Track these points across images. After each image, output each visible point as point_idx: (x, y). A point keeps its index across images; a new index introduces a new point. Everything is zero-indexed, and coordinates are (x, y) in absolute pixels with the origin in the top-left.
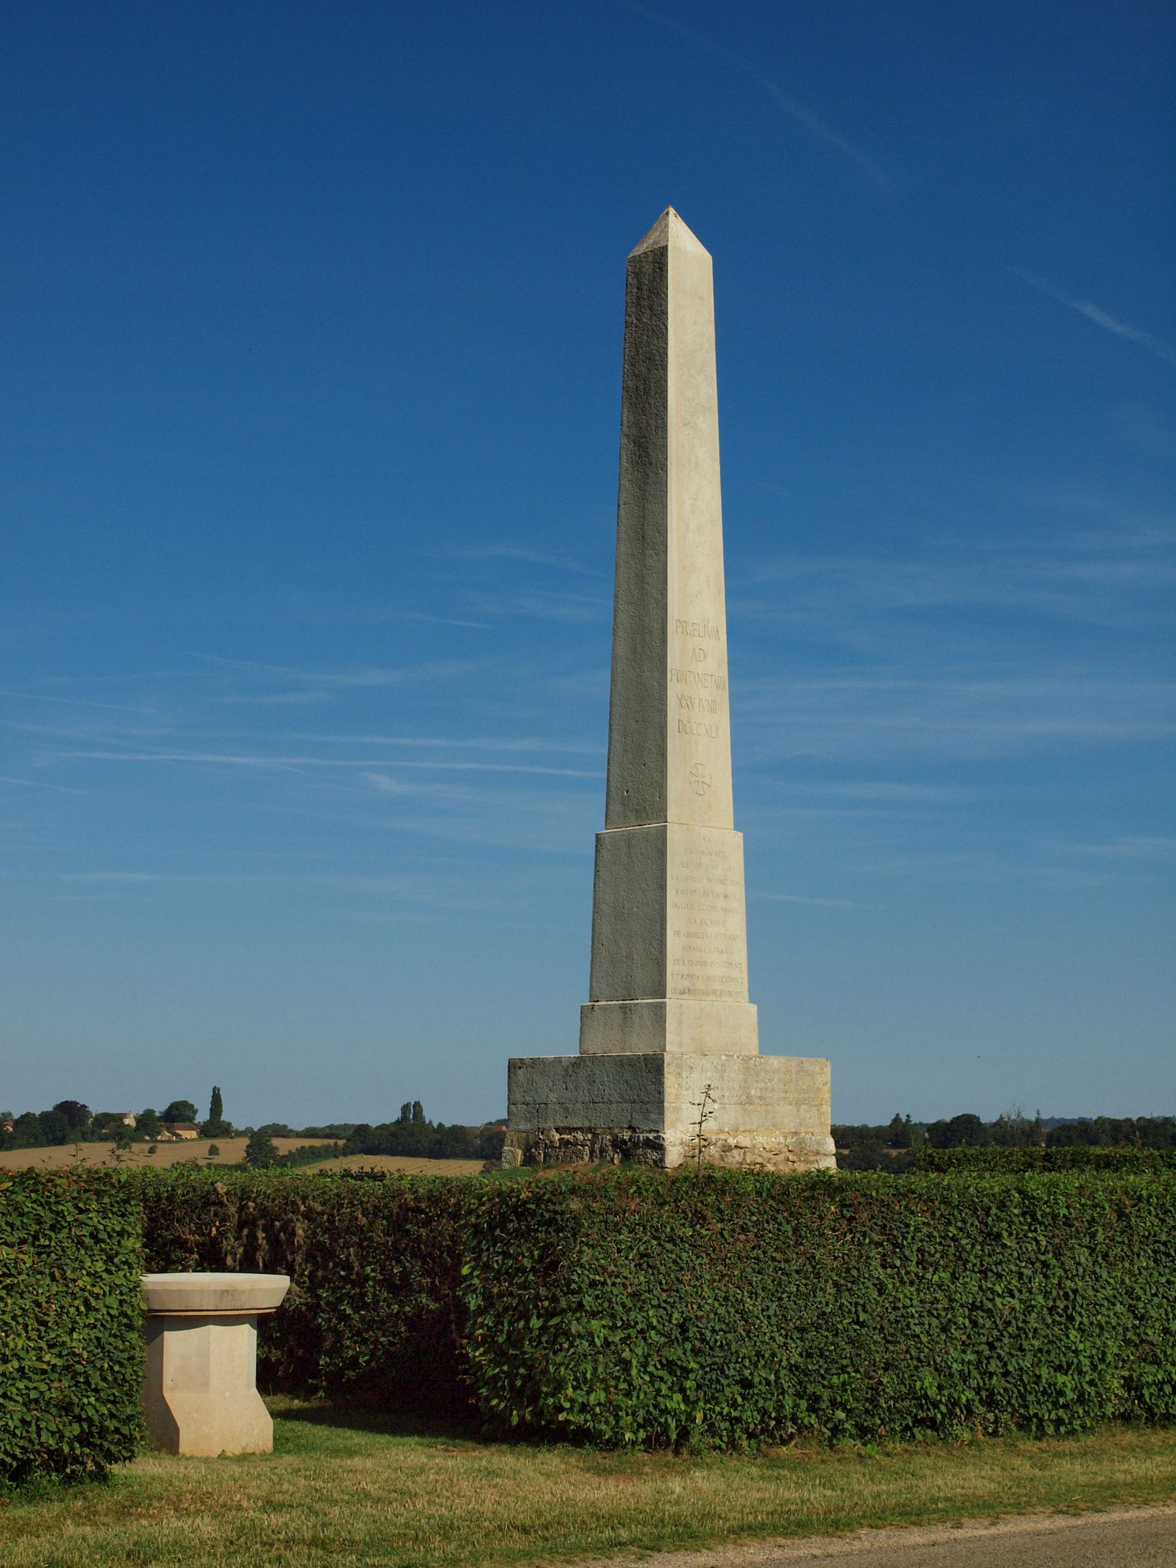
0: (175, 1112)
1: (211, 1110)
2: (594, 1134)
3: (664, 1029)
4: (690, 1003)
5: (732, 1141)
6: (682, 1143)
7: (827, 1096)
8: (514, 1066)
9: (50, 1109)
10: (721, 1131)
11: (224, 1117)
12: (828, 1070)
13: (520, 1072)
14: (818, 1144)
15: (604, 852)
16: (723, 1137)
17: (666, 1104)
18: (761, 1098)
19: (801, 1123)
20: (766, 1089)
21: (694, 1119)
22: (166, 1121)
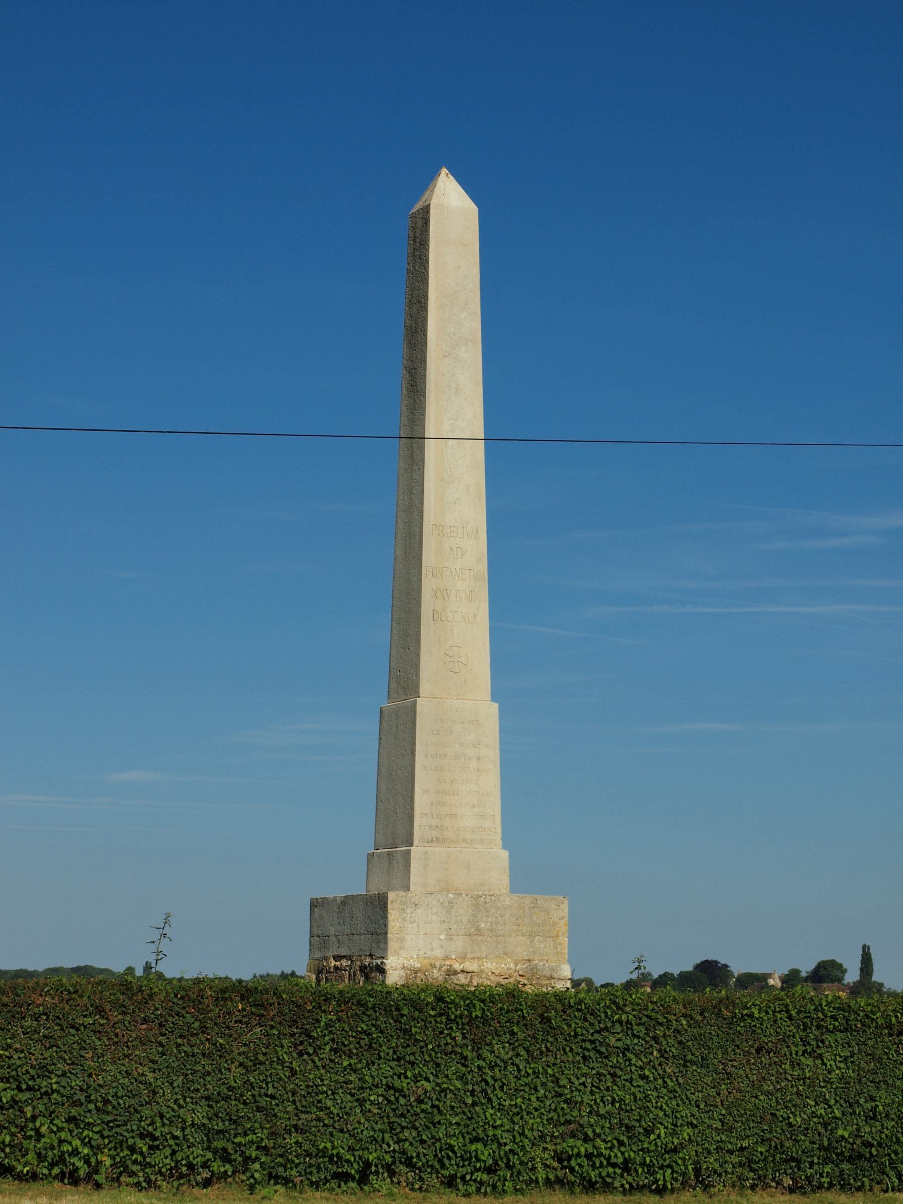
0: (822, 972)
1: (862, 970)
2: (352, 961)
3: (409, 872)
4: (437, 851)
5: (457, 967)
6: (403, 968)
7: (564, 928)
8: (314, 904)
9: (690, 968)
10: (447, 958)
11: (876, 977)
12: (565, 906)
13: (316, 909)
14: (552, 969)
15: (384, 724)
16: (448, 962)
17: (389, 935)
18: (491, 930)
20: (497, 923)
21: (418, 947)
22: (813, 982)
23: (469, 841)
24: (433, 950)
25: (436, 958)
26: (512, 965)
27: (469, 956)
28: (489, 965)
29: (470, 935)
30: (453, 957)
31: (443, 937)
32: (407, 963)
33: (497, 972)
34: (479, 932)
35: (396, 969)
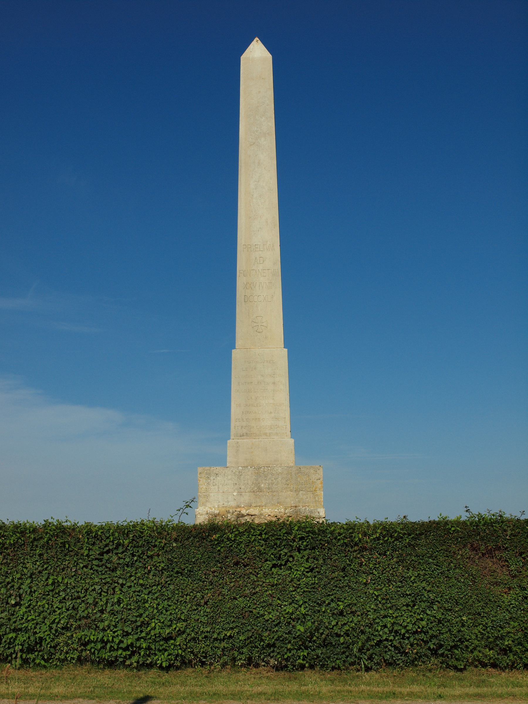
5: (244, 512)
6: (207, 514)
10: (238, 507)
12: (321, 472)
16: (238, 510)
18: (269, 489)
19: (299, 502)
20: (272, 484)
23: (268, 435)
24: (228, 502)
25: (231, 507)
26: (283, 510)
27: (254, 505)
28: (267, 510)
29: (254, 492)
30: (243, 506)
31: (235, 494)
32: (209, 511)
33: (272, 515)
34: (260, 490)
35: (202, 515)
